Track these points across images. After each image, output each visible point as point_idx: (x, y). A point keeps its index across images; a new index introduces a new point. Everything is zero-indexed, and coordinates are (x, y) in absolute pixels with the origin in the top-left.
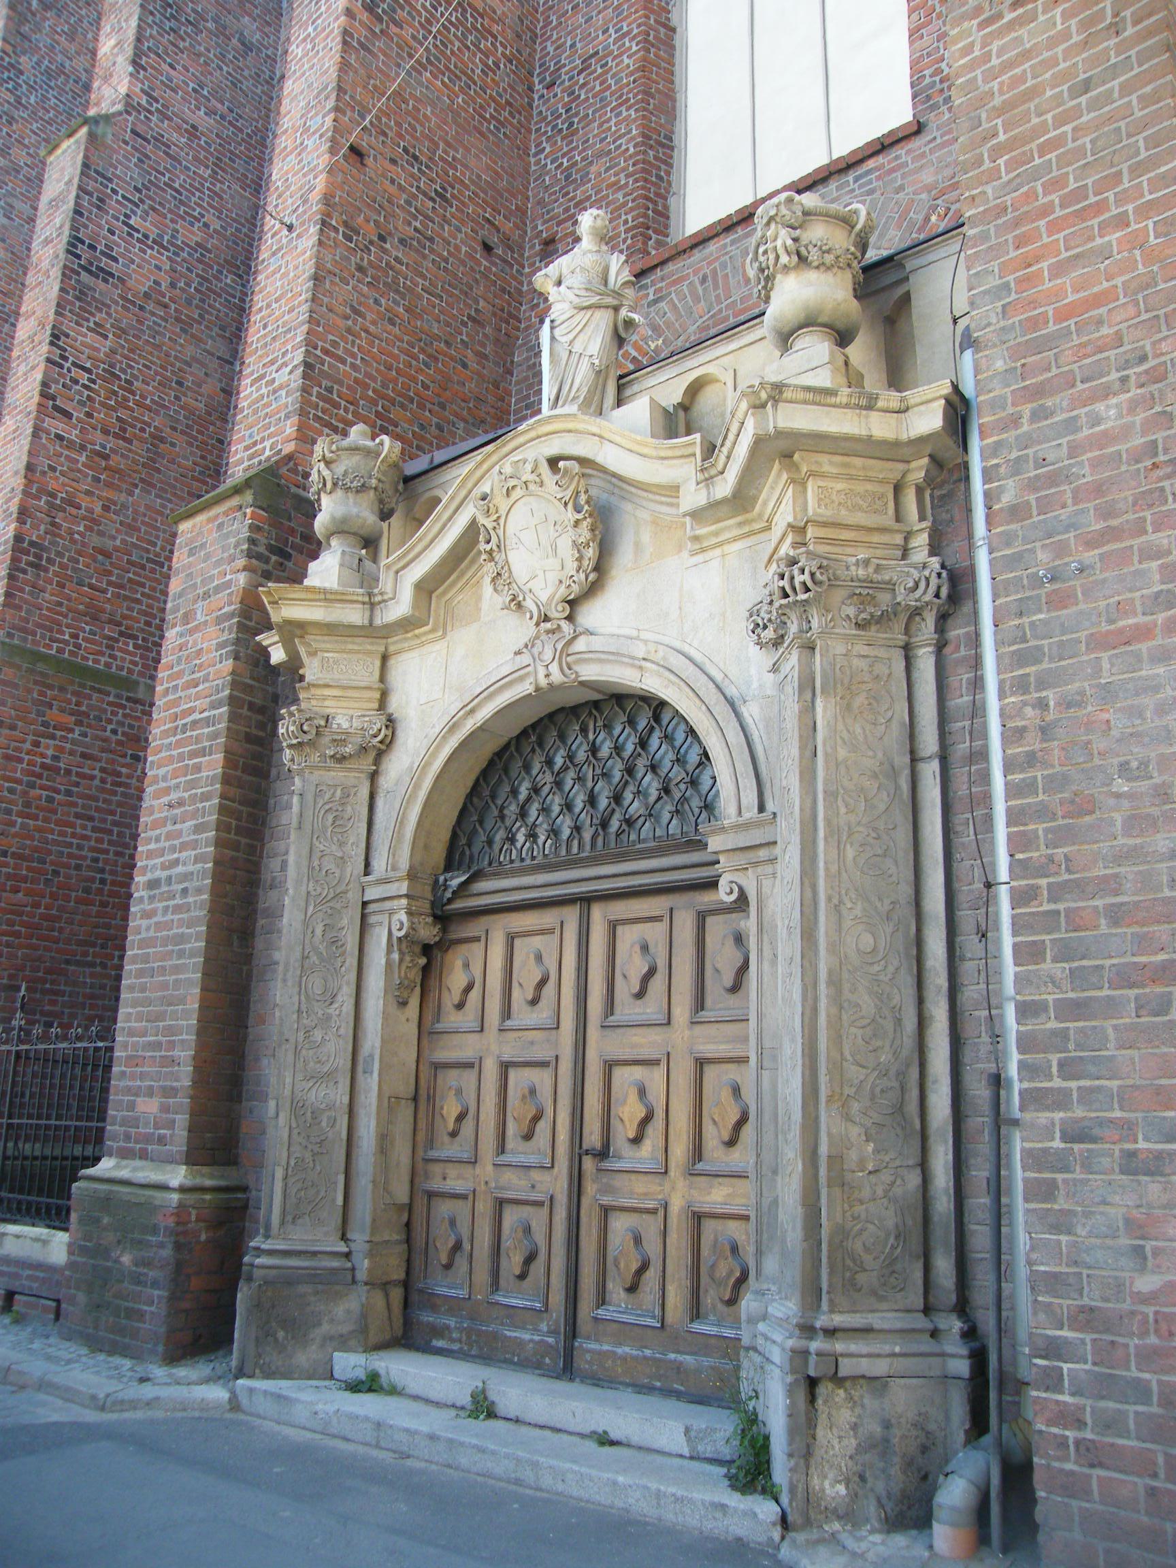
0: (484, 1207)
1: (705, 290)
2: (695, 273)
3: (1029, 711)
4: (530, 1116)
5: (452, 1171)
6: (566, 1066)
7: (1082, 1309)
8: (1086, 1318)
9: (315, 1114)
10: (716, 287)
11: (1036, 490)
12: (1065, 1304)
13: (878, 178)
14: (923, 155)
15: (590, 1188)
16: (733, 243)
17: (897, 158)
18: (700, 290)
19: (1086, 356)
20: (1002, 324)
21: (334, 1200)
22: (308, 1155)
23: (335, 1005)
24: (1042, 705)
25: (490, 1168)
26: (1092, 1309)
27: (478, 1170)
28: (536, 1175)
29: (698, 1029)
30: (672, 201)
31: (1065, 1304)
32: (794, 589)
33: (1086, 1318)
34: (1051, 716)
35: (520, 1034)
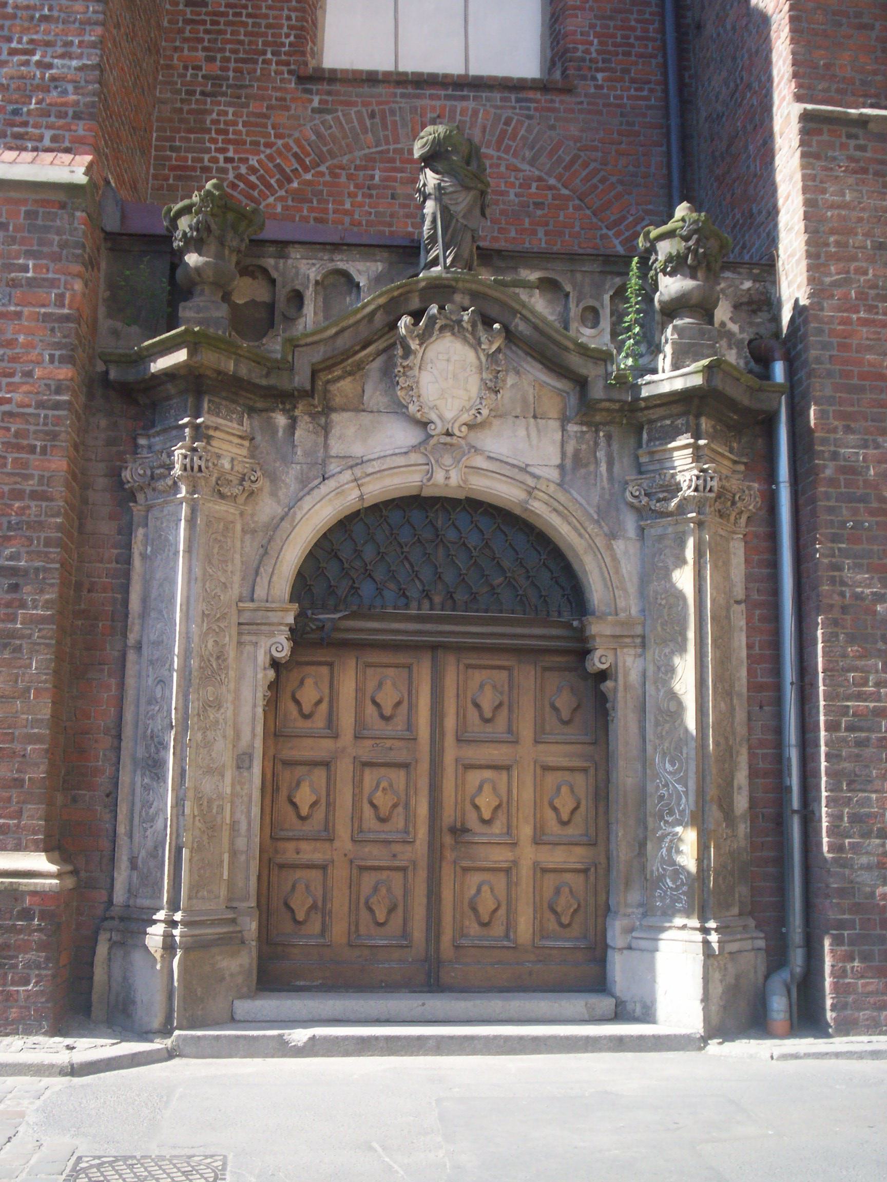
0: (340, 873)
1: (372, 124)
2: (364, 104)
3: (836, 597)
4: (390, 804)
5: (304, 846)
6: (424, 767)
7: (855, 904)
8: (856, 908)
9: (210, 801)
10: (385, 127)
11: (844, 473)
12: (846, 902)
13: (536, 109)
14: (572, 111)
15: (449, 855)
16: (403, 96)
17: (552, 101)
18: (368, 122)
19: (873, 407)
20: (828, 366)
21: (222, 875)
22: (205, 838)
23: (222, 710)
24: (842, 594)
25: (349, 846)
26: (859, 904)
27: (337, 844)
28: (397, 848)
29: (541, 747)
30: (319, 13)
31: (846, 902)
32: (705, 488)
33: (856, 908)
34: (847, 601)
35: (378, 741)
